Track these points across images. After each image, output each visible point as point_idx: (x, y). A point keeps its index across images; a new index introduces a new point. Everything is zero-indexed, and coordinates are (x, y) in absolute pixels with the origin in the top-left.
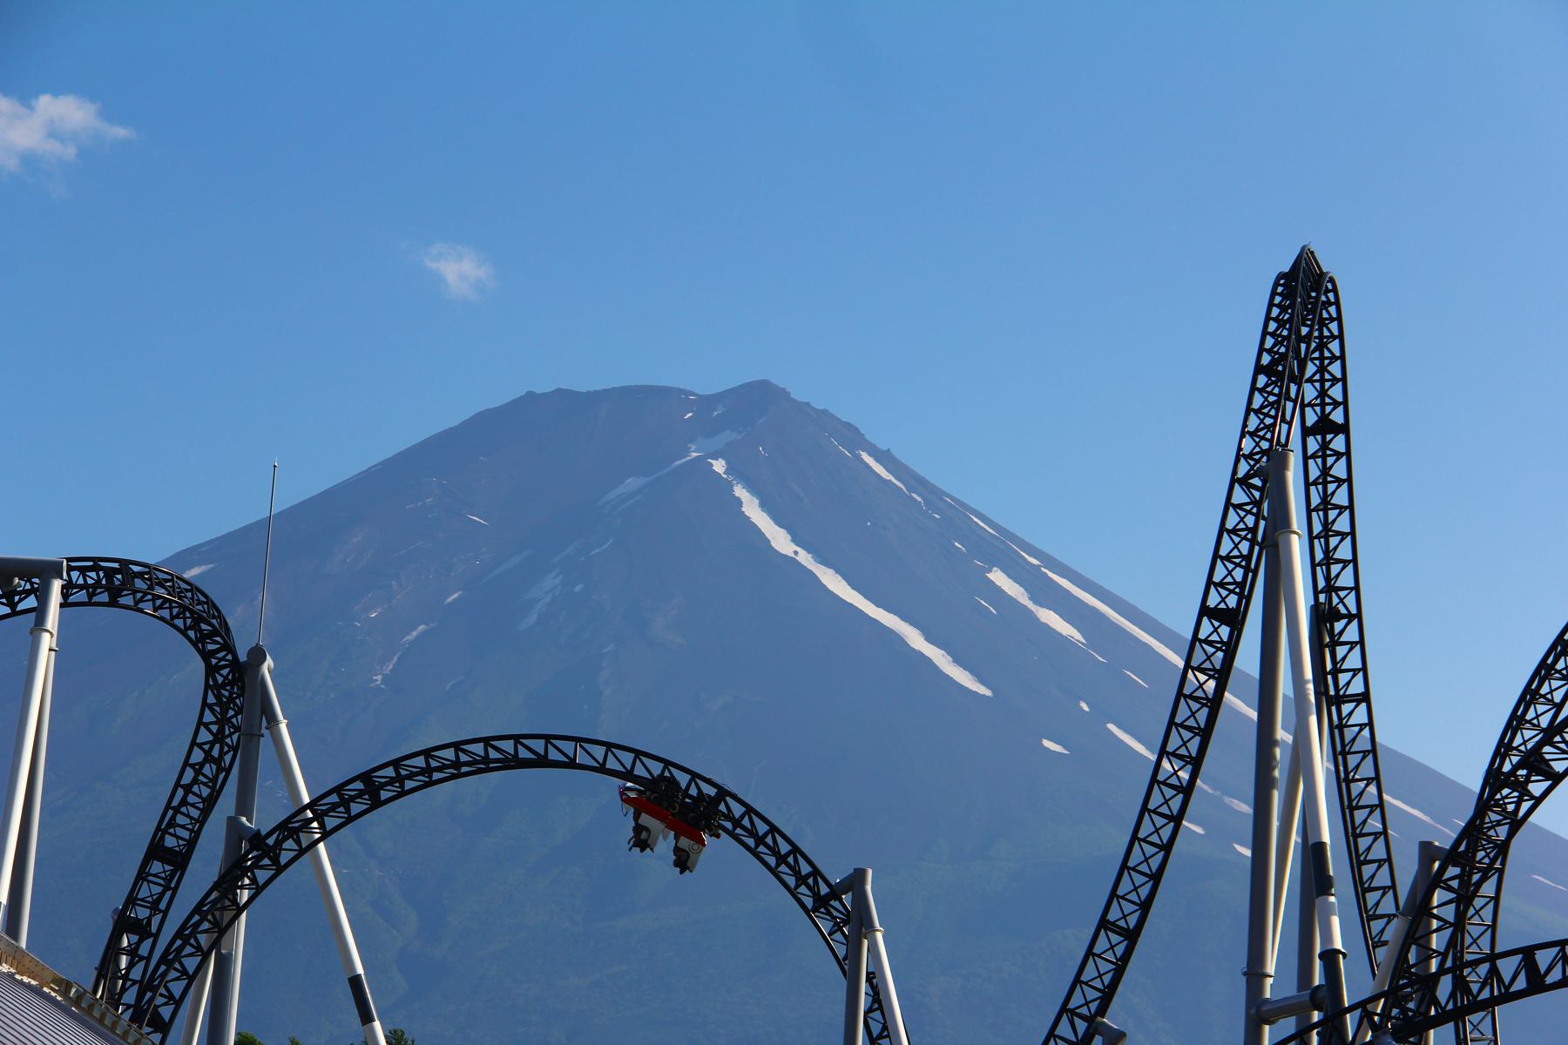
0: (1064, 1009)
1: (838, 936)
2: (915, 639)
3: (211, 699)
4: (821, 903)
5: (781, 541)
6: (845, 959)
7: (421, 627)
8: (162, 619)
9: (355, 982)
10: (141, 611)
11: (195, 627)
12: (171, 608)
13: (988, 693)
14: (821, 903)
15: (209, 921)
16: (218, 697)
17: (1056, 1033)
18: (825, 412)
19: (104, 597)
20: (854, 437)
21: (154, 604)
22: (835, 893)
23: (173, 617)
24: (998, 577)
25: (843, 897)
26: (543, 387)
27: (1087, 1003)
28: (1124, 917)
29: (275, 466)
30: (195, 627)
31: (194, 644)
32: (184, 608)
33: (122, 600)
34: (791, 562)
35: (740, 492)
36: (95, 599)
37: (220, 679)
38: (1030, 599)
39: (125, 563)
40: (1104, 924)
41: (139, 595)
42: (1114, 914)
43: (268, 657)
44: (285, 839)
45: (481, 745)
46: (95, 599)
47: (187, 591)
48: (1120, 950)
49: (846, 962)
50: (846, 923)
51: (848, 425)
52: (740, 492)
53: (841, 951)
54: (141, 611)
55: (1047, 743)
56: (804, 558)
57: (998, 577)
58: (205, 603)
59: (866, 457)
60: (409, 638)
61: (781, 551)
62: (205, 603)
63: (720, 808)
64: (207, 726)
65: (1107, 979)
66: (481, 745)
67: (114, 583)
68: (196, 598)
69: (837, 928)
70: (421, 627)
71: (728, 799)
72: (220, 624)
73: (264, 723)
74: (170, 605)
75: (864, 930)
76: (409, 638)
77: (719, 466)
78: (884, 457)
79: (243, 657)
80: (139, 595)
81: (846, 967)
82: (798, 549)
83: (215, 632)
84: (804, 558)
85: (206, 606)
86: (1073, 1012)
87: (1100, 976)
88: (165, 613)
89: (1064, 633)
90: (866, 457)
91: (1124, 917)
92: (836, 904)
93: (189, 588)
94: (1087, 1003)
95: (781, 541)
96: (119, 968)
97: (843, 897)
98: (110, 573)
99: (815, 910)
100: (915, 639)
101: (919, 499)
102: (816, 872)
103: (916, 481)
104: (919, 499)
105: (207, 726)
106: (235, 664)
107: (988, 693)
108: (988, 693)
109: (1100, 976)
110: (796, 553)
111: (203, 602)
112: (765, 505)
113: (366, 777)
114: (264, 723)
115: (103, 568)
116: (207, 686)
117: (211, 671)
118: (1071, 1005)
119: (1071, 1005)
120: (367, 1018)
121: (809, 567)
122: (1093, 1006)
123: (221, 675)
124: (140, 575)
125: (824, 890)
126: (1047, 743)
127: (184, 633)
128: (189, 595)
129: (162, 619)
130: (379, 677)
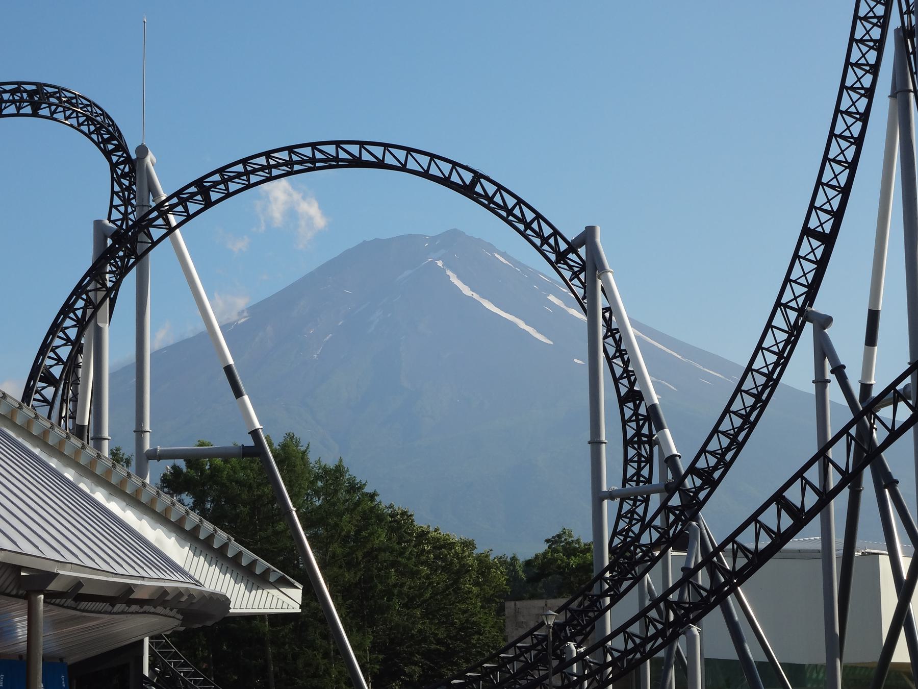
0: (778, 304)
1: (576, 281)
2: (522, 325)
3: (117, 188)
4: (562, 257)
5: (467, 291)
6: (583, 299)
7: (330, 335)
8: (71, 126)
9: (228, 370)
10: (56, 120)
11: (97, 131)
12: (77, 117)
13: (551, 343)
14: (562, 257)
15: (83, 299)
16: (120, 184)
17: (773, 324)
18: (479, 239)
19: (28, 110)
20: (492, 248)
21: (65, 115)
22: (572, 248)
23: (80, 125)
24: (552, 298)
25: (579, 250)
26: (369, 238)
27: (795, 298)
28: (821, 225)
29: (144, 22)
30: (97, 131)
31: (98, 144)
32: (88, 119)
33: (41, 112)
34: (471, 298)
35: (449, 273)
36: (22, 111)
37: (119, 172)
38: (565, 305)
39: (40, 86)
40: (806, 232)
41: (53, 108)
42: (813, 224)
43: (150, 152)
44: (139, 232)
45: (286, 152)
46: (22, 111)
47: (88, 105)
48: (819, 253)
49: (585, 301)
50: (583, 268)
51: (489, 243)
52: (449, 273)
53: (580, 292)
54: (56, 120)
55: (576, 360)
56: (476, 296)
57: (552, 298)
58: (101, 115)
59: (497, 255)
60: (325, 340)
61: (467, 295)
62: (101, 115)
63: (476, 190)
64: (116, 207)
65: (810, 277)
66: (286, 152)
67: (34, 99)
68: (94, 111)
69: (576, 275)
70: (330, 335)
71: (482, 180)
72: (114, 130)
73: (151, 198)
74: (77, 115)
75: (597, 273)
76: (325, 340)
77: (440, 263)
78: (503, 255)
79: (134, 156)
80: (53, 108)
81: (586, 305)
82: (473, 293)
83: (112, 138)
84: (476, 296)
85: (102, 117)
86: (786, 306)
87: (805, 275)
88: (74, 122)
89: (579, 317)
90: (497, 255)
91: (821, 225)
92: (572, 256)
93: (89, 103)
94: (795, 298)
95: (467, 291)
96: (78, 377)
97: (579, 250)
98: (31, 94)
99: (558, 261)
100: (522, 325)
101: (519, 270)
102: (556, 233)
103: (517, 263)
104: (519, 270)
105: (116, 207)
106: (128, 160)
107: (551, 343)
108: (551, 343)
109: (805, 275)
110: (473, 295)
111: (100, 114)
112: (459, 277)
113: (199, 183)
114: (151, 198)
115: (25, 91)
116: (113, 179)
117: (113, 167)
118: (784, 301)
119: (784, 301)
120: (238, 393)
121: (477, 299)
122: (801, 300)
123: (119, 169)
124: (52, 95)
125: (563, 246)
126: (576, 360)
127: (88, 135)
128: (89, 108)
129: (71, 126)
130: (316, 356)
